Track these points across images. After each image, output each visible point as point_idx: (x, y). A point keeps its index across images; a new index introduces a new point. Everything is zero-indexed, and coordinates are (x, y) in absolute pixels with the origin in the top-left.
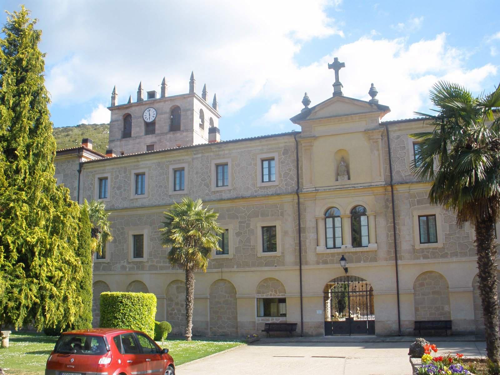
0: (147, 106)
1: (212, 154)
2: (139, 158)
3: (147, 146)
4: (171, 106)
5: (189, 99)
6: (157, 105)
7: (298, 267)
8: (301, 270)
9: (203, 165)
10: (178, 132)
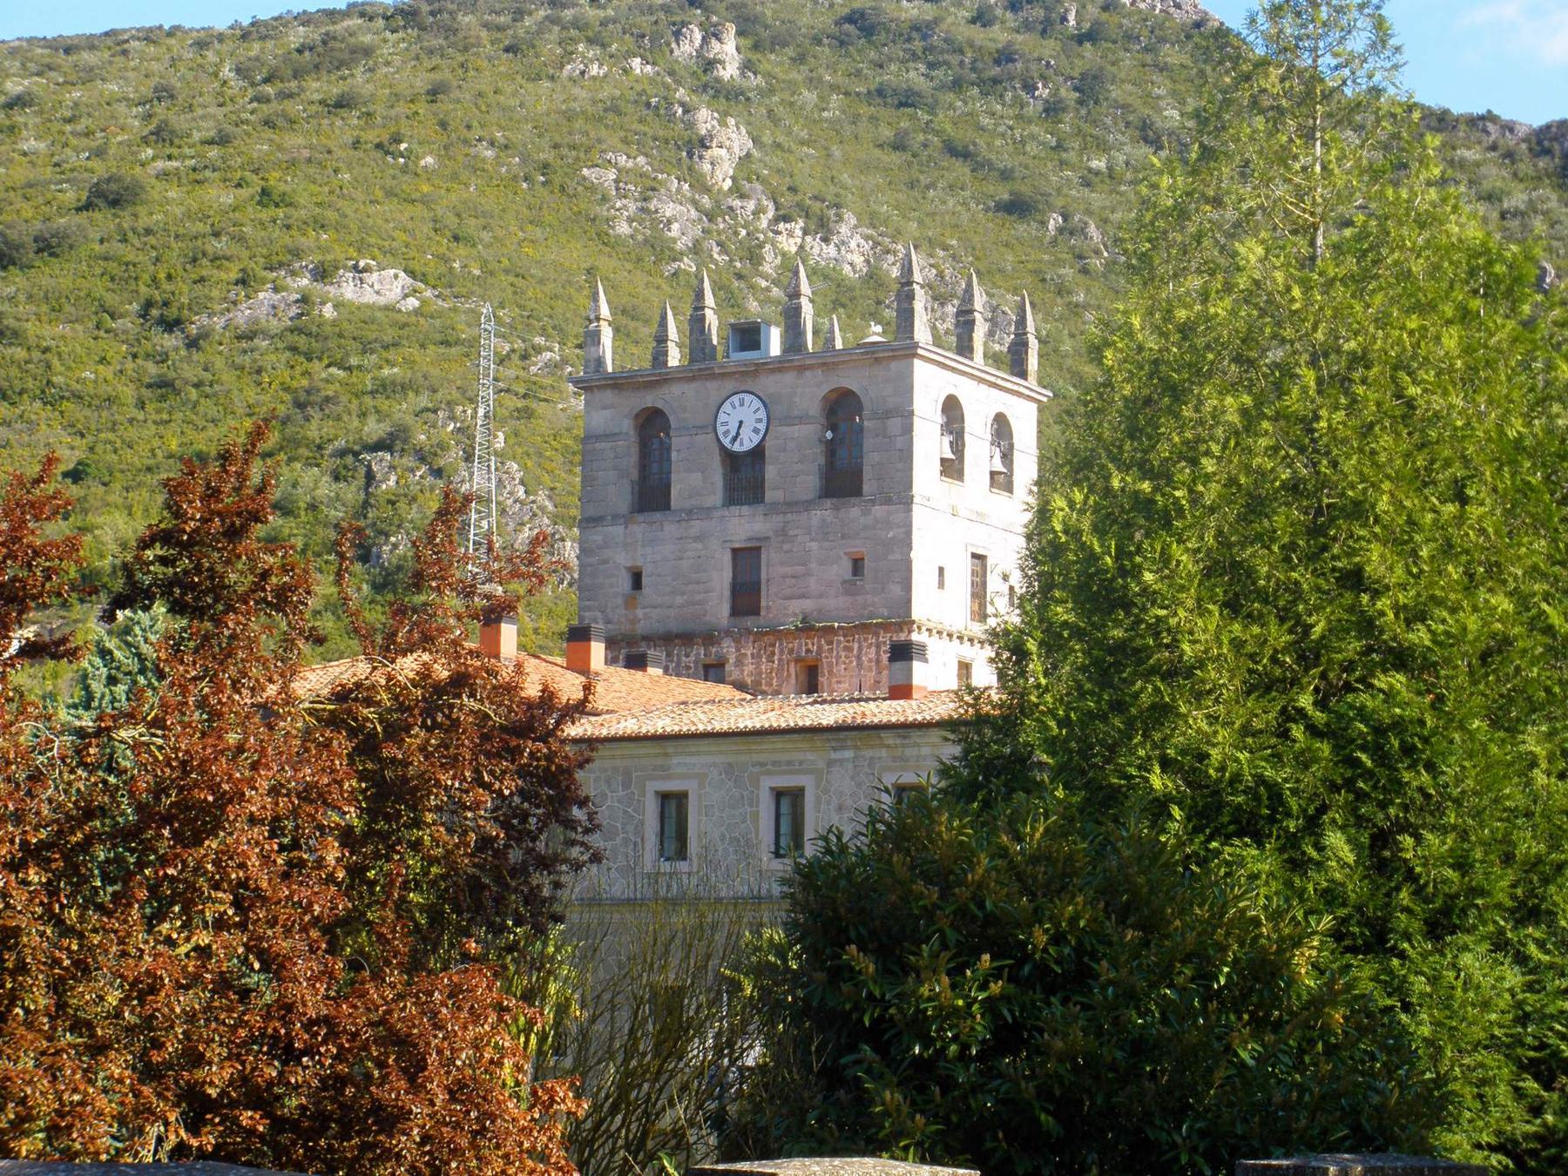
0: (730, 385)
1: (884, 753)
2: (670, 747)
3: (735, 551)
5: (894, 365)
6: (769, 383)
9: (859, 785)
10: (853, 500)
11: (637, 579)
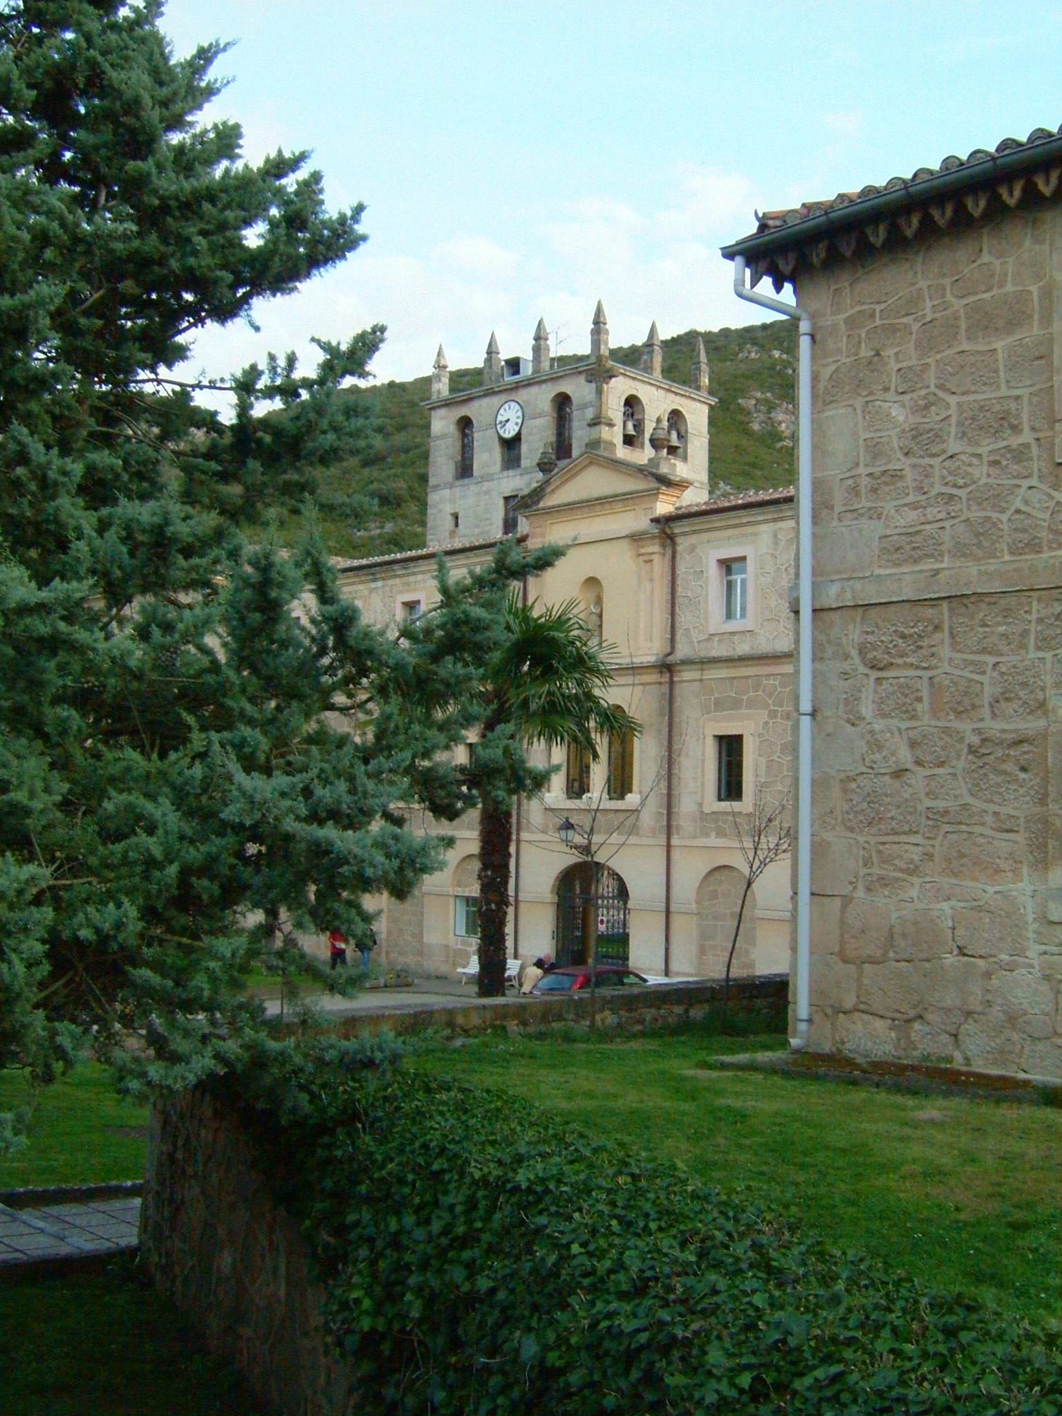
0: (503, 397)
1: (398, 581)
4: (553, 394)
7: (663, 840)
8: (669, 847)
11: (456, 517)
